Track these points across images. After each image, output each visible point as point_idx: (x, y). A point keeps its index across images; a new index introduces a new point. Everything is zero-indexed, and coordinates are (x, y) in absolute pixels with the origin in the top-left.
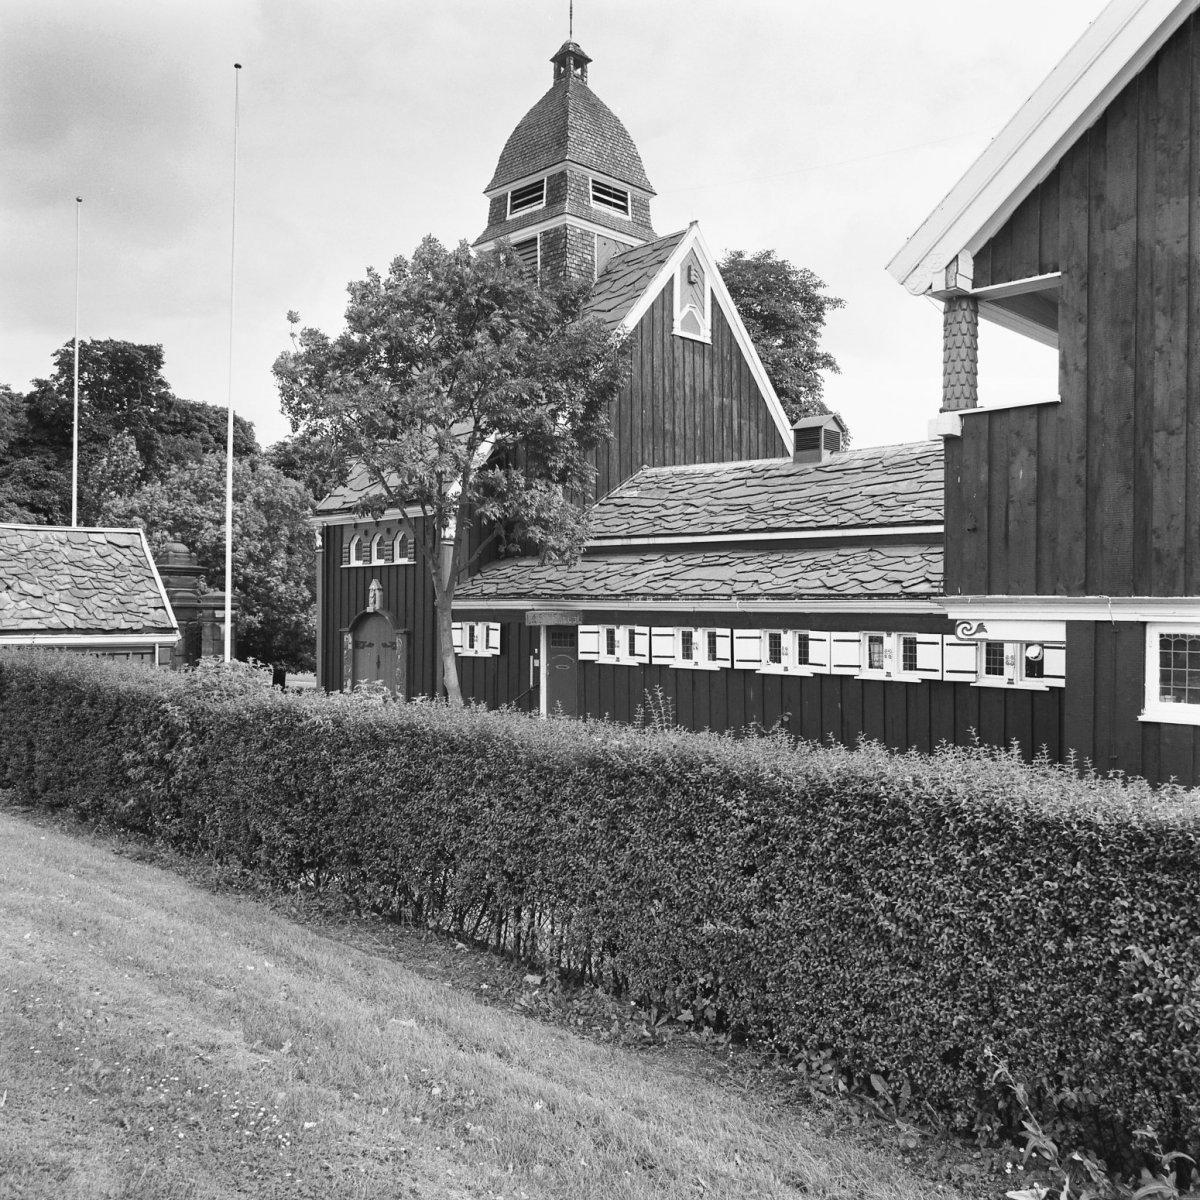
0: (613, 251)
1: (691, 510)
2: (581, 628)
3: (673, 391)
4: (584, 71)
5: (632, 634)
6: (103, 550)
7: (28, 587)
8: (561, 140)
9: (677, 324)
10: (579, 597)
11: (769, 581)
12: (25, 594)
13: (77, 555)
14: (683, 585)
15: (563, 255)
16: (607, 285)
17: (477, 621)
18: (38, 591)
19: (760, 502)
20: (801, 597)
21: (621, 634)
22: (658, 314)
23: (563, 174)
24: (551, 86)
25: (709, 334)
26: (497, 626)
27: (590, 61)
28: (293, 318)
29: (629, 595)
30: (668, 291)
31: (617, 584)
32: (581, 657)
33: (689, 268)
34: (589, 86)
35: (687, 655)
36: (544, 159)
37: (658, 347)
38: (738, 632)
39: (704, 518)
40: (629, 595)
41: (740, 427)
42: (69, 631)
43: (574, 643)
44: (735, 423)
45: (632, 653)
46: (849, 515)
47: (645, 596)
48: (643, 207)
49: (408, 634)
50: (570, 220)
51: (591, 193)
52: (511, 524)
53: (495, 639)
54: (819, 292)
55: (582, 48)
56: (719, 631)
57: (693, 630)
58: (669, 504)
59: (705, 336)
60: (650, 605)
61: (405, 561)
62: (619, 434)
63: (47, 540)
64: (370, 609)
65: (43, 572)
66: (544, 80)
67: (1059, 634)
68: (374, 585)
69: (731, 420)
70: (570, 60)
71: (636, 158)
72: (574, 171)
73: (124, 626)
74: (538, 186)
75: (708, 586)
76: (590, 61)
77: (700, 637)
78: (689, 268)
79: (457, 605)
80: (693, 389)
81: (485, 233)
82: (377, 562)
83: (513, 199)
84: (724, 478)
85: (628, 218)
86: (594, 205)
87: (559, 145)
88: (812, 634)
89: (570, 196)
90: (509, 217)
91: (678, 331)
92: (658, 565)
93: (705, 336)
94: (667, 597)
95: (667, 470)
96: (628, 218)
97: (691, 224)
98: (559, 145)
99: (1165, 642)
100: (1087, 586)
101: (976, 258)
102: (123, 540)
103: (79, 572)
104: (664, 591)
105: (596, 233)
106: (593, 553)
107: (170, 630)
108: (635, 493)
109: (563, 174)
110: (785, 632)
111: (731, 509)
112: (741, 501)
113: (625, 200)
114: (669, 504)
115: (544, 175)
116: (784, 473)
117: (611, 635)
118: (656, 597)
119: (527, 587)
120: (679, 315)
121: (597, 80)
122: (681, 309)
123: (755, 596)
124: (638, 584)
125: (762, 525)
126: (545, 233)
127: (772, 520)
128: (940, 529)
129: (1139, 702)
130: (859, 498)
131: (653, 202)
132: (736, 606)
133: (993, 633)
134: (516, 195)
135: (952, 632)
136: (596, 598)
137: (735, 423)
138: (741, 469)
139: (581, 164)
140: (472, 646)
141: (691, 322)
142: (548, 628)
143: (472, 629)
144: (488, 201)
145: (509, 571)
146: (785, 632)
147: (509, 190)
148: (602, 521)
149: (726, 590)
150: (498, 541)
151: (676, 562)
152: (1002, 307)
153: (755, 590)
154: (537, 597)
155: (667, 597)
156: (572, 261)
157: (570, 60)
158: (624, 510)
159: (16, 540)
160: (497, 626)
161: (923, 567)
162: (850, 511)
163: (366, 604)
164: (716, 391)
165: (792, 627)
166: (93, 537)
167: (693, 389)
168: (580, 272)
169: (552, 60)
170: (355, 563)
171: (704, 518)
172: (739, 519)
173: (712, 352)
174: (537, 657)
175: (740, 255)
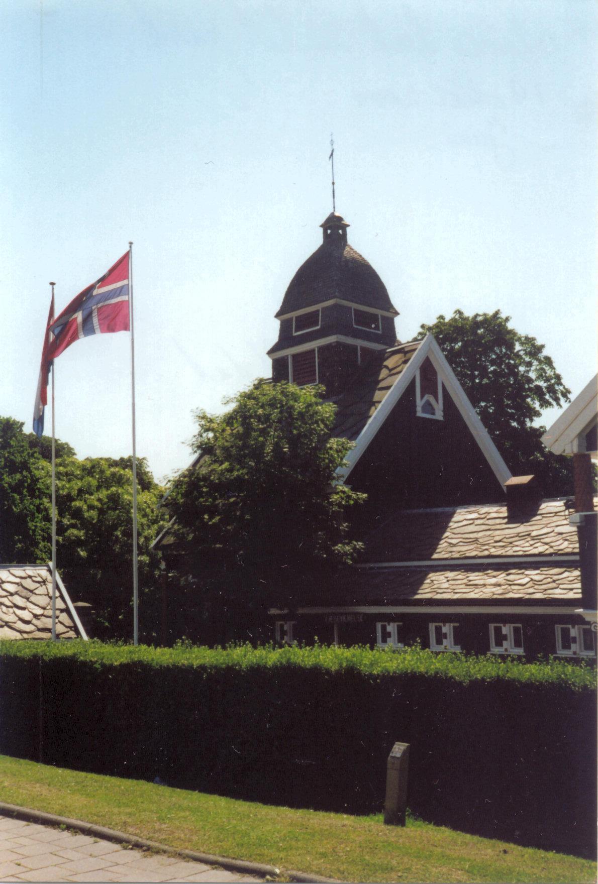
9: (419, 409)
25: (442, 413)
27: (348, 226)
46: (547, 547)
57: (570, 626)
76: (348, 226)
91: (420, 413)
93: (439, 415)
97: (61, 333)
110: (573, 627)
112: (472, 536)
120: (420, 403)
122: (437, 400)
127: (493, 550)
128: (577, 558)
130: (552, 534)
141: (428, 408)
146: (573, 627)
152: (408, 387)
162: (546, 544)
165: (510, 622)
169: (321, 226)
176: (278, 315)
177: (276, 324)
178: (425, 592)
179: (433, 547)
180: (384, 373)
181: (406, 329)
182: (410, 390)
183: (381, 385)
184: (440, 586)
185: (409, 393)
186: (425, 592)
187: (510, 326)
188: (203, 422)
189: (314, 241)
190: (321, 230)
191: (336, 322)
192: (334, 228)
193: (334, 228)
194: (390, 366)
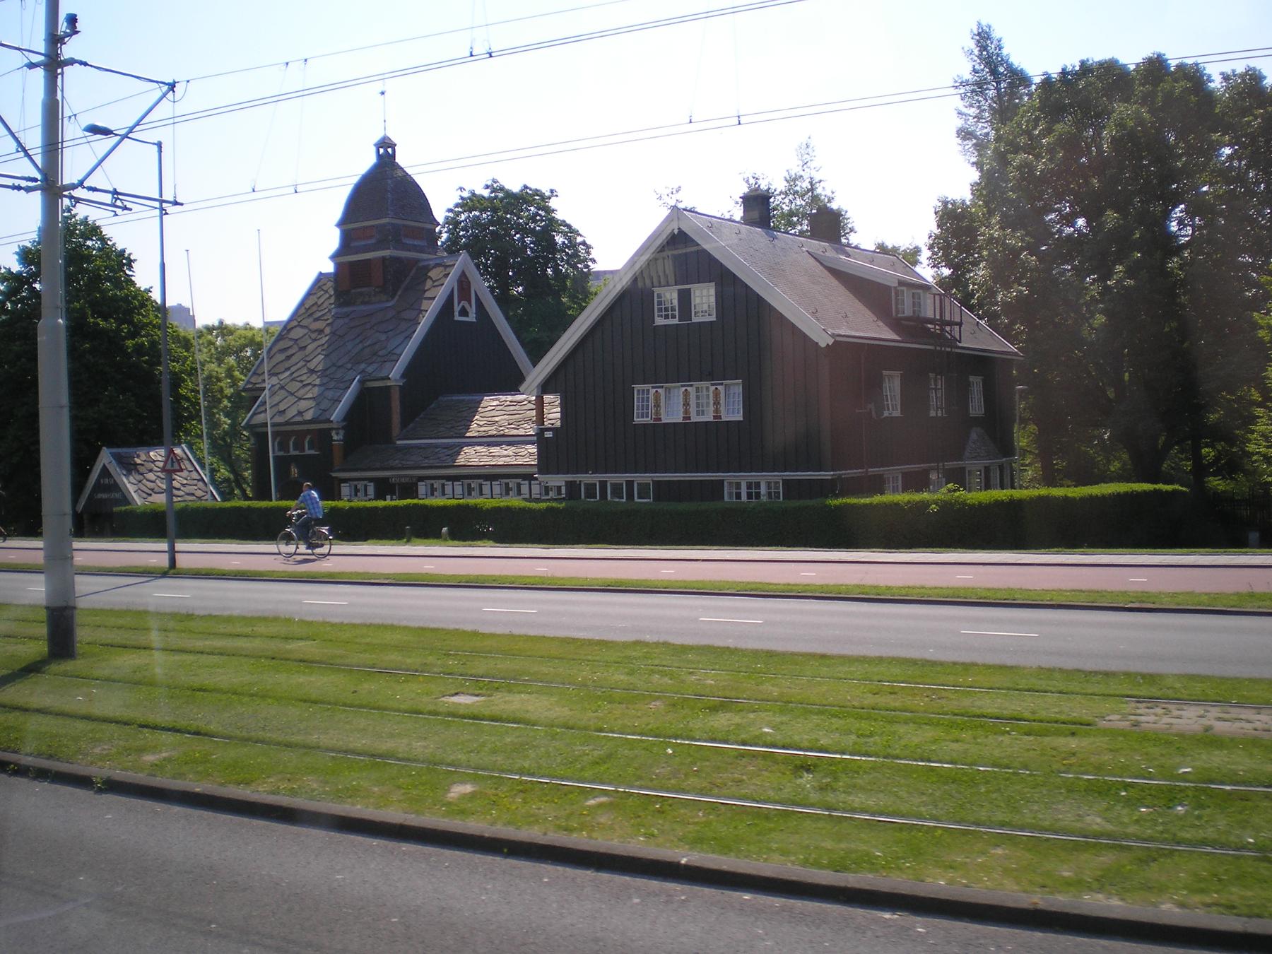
9: (456, 314)
59: (472, 317)
61: (312, 452)
82: (293, 452)
91: (457, 318)
93: (472, 317)
120: (457, 308)
176: (339, 225)
177: (337, 233)
178: (461, 460)
179: (468, 428)
180: (429, 283)
181: (440, 214)
182: (450, 299)
183: (427, 294)
184: (472, 456)
185: (448, 306)
186: (461, 460)
187: (834, 206)
188: (962, 91)
189: (368, 160)
190: (374, 149)
191: (393, 236)
192: (386, 148)
193: (386, 148)
194: (183, 561)
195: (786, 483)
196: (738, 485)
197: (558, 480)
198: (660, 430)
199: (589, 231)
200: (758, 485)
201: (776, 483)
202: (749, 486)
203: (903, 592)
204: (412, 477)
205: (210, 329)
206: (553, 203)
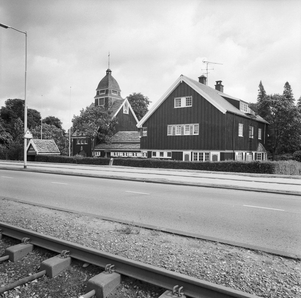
0: (115, 100)
1: (125, 138)
2: (111, 152)
3: (123, 121)
4: (111, 73)
5: (117, 153)
6: (50, 143)
7: (43, 147)
8: (107, 85)
9: (124, 112)
10: (111, 149)
11: (133, 147)
12: (43, 148)
13: (47, 143)
14: (123, 147)
15: (108, 101)
16: (114, 106)
17: (97, 152)
18: (44, 148)
19: (133, 137)
20: (136, 149)
21: (116, 153)
22: (121, 111)
23: (108, 90)
24: (106, 75)
26: (100, 152)
28: (74, 115)
29: (117, 149)
30: (122, 108)
31: (115, 147)
32: (111, 156)
33: (126, 104)
34: (111, 75)
35: (124, 155)
36: (105, 87)
37: (121, 115)
38: (129, 153)
39: (126, 139)
40: (117, 149)
41: (133, 125)
42: (48, 153)
43: (110, 154)
44: (132, 125)
45: (117, 155)
47: (119, 149)
48: (119, 93)
49: (87, 153)
50: (109, 96)
51: (112, 92)
52: (103, 140)
53: (100, 154)
54: (148, 100)
55: (111, 70)
56: (127, 153)
58: (122, 137)
59: (128, 113)
60: (119, 150)
61: (86, 144)
62: (116, 129)
63: (43, 141)
64: (81, 150)
65: (44, 146)
66: (105, 74)
67: (147, 152)
68: (82, 147)
69: (131, 125)
70: (109, 72)
71: (118, 86)
72: (109, 89)
73: (54, 152)
74: (104, 90)
75: (126, 148)
77: (125, 153)
78: (126, 104)
79: (95, 150)
80: (126, 120)
81: (96, 96)
82: (82, 144)
83: (100, 92)
84: (129, 134)
85: (117, 95)
86: (112, 93)
87: (106, 85)
88: (137, 153)
89: (109, 92)
90: (100, 94)
92: (121, 145)
93: (128, 113)
94: (121, 149)
95: (122, 132)
96: (117, 95)
98: (106, 85)
99: (153, 152)
100: (148, 149)
101: (142, 125)
102: (52, 141)
103: (48, 145)
104: (121, 148)
105: (112, 97)
106: (113, 143)
107: (59, 153)
108: (118, 135)
109: (108, 90)
111: (130, 138)
113: (117, 92)
114: (122, 137)
115: (105, 89)
116: (136, 133)
117: (115, 153)
118: (120, 149)
119: (104, 147)
120: (124, 110)
121: (113, 74)
123: (131, 149)
124: (118, 147)
125: (133, 140)
126: (105, 98)
129: (151, 156)
131: (121, 92)
132: (129, 150)
133: (143, 152)
134: (101, 91)
135: (141, 152)
136: (113, 149)
137: (132, 125)
138: (131, 132)
139: (110, 87)
140: (96, 155)
142: (107, 152)
143: (96, 153)
144: (96, 91)
145: (101, 145)
147: (100, 90)
148: (113, 139)
149: (128, 148)
150: (99, 141)
151: (123, 145)
153: (131, 148)
154: (105, 149)
155: (121, 149)
156: (109, 102)
157: (109, 72)
158: (116, 137)
159: (40, 142)
160: (100, 152)
161: (138, 146)
163: (80, 149)
164: (129, 120)
166: (48, 141)
167: (126, 120)
168: (110, 103)
170: (78, 144)
171: (126, 139)
172: (130, 139)
173: (129, 115)
174: (105, 156)
175: (135, 93)
189: (199, 79)
192: (198, 78)
195: (172, 152)
196: (197, 154)
197: (145, 151)
198: (175, 138)
199: (277, 93)
200: (202, 154)
201: (260, 154)
202: (200, 154)
203: (204, 184)
204: (109, 151)
205: (269, 97)
206: (259, 89)
